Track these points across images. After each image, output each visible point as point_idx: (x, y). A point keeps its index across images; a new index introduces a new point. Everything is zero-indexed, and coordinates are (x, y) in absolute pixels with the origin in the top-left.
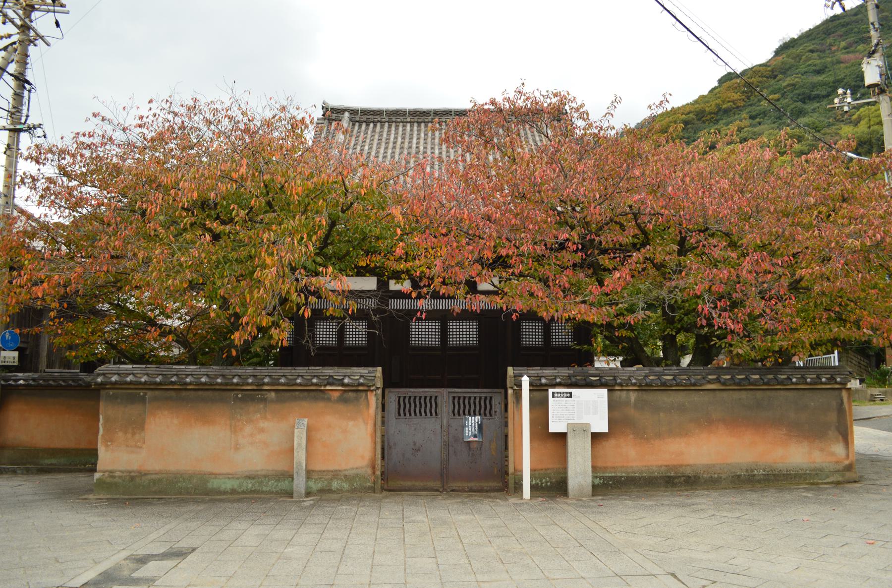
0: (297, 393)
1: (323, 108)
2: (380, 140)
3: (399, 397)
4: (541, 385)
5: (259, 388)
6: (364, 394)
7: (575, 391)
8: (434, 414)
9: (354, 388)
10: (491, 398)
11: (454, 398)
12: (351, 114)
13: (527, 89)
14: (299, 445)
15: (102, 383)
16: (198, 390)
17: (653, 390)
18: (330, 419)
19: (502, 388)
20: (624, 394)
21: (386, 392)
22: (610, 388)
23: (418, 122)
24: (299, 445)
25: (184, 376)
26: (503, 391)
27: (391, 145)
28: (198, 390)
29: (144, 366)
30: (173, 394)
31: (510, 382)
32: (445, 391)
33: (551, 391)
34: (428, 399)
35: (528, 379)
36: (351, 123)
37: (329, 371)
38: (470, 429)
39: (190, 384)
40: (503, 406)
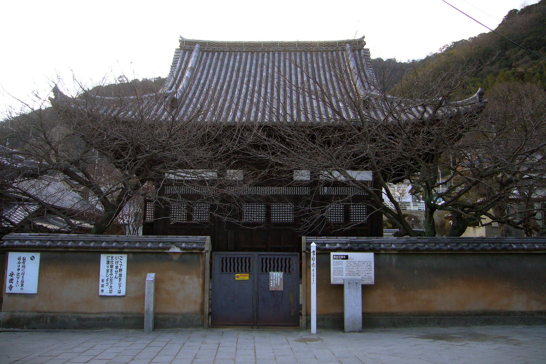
0: (148, 255)
1: (180, 41)
2: (222, 65)
3: (223, 258)
4: (326, 249)
5: (120, 250)
6: (196, 256)
7: (350, 254)
8: (248, 271)
9: (190, 251)
10: (290, 259)
11: (263, 259)
12: (201, 45)
13: (144, 78)
14: (149, 292)
15: (7, 246)
16: (77, 252)
17: (409, 254)
18: (171, 274)
19: (297, 252)
20: (388, 257)
21: (213, 254)
22: (377, 252)
23: (251, 52)
24: (149, 292)
25: (67, 242)
26: (298, 254)
27: (230, 69)
28: (77, 252)
29: (38, 234)
30: (59, 255)
31: (304, 248)
32: (256, 254)
33: (332, 254)
34: (244, 259)
35: (315, 245)
36: (201, 52)
37: (170, 238)
38: (274, 282)
39: (71, 247)
40: (298, 265)
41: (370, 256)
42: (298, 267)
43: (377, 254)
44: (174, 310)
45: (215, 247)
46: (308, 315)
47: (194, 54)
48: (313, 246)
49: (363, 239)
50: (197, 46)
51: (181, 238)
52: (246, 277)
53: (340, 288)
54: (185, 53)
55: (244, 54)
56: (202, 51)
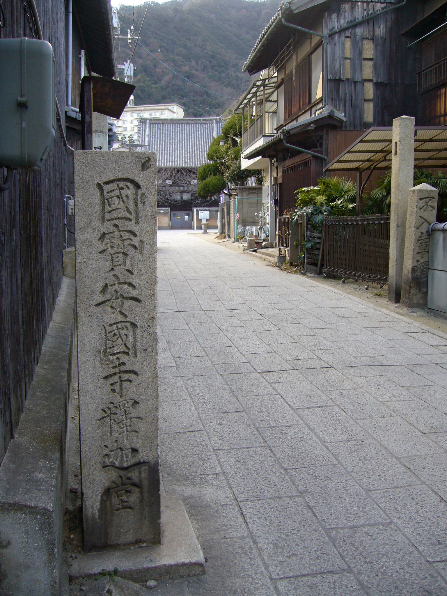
37: (160, 208)
41: (209, 212)
42: (155, 108)
43: (210, 211)
44: (162, 226)
45: (171, 210)
46: (194, 226)
47: (147, 125)
48: (195, 210)
49: (207, 208)
50: (148, 121)
51: (163, 208)
52: (179, 218)
53: (201, 220)
54: (143, 124)
55: (169, 125)
56: (150, 123)
